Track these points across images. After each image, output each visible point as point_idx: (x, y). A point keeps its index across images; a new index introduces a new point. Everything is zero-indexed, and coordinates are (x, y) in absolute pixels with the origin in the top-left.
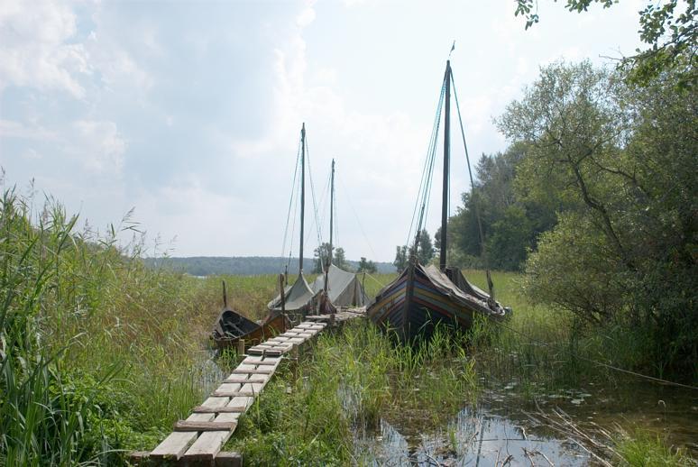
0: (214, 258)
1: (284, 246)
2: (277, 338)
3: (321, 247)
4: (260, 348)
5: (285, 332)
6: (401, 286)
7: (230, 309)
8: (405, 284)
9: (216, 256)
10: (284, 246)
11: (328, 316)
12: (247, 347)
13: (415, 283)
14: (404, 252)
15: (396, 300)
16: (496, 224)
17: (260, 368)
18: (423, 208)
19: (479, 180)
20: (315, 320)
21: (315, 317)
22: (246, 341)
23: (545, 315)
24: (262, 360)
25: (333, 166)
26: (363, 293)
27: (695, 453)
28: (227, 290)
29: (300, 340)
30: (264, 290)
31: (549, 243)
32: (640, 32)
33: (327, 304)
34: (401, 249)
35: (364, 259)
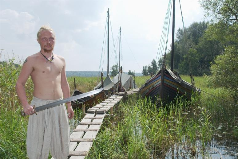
0: (71, 72)
1: (101, 59)
2: (101, 104)
3: (113, 67)
4: (93, 109)
5: (104, 101)
6: (158, 78)
7: (77, 90)
8: (160, 77)
9: (72, 71)
10: (101, 59)
11: (123, 93)
12: (87, 109)
13: (165, 77)
14: (146, 68)
15: (155, 85)
16: (184, 56)
17: (95, 121)
18: (167, 42)
19: (177, 39)
20: (117, 95)
21: (117, 93)
22: (86, 105)
23: (218, 91)
24: (95, 116)
25: (120, 30)
26: (135, 84)
27: (4, 63)
28: (76, 83)
29: (113, 105)
30: (92, 82)
31: (221, 59)
32: (37, 114)
33: (121, 87)
34: (145, 67)
35: (130, 71)
